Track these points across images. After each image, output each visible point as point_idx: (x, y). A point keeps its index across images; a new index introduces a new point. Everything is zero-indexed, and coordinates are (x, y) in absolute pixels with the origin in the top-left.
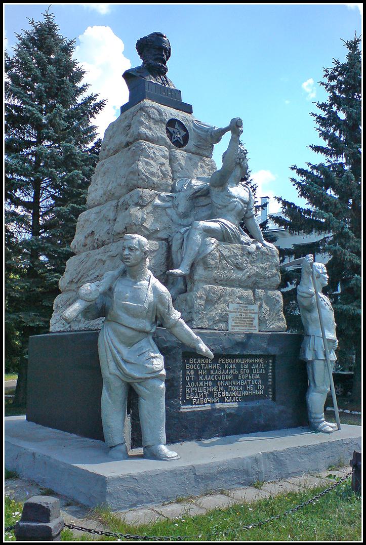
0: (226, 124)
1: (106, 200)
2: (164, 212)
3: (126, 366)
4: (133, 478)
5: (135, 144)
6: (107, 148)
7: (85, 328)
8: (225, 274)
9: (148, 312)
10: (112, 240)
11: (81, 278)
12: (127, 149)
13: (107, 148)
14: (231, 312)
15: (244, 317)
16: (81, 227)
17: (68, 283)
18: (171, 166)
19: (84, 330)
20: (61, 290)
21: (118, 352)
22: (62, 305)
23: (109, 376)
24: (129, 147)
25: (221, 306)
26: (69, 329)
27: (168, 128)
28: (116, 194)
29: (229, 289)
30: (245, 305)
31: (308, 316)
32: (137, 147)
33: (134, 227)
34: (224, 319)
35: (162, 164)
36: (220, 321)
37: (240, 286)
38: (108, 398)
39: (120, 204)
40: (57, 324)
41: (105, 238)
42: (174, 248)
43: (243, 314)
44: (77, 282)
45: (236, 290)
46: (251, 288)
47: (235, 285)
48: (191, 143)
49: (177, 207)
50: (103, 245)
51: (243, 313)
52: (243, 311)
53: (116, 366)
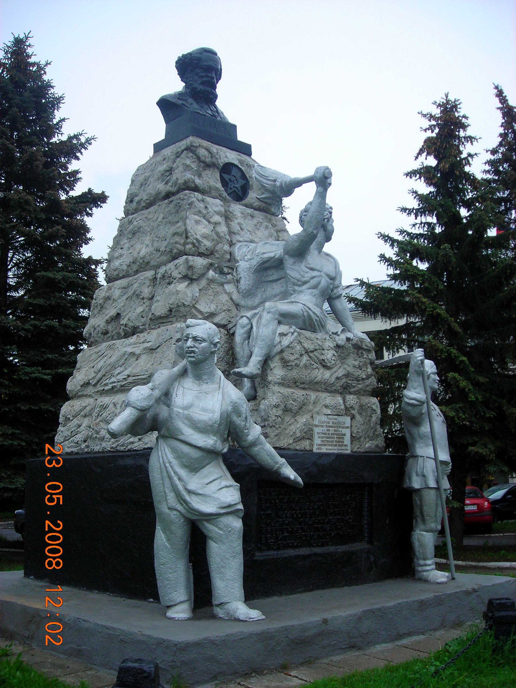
0: (310, 172)
1: (137, 270)
2: (221, 287)
3: (190, 498)
4: (212, 642)
5: (181, 195)
6: (137, 199)
7: (112, 448)
8: (305, 375)
9: (220, 425)
10: (147, 326)
11: (101, 379)
12: (166, 201)
13: (137, 199)
14: (317, 426)
15: (333, 432)
16: (99, 307)
17: (81, 386)
18: (228, 226)
19: (110, 451)
20: (71, 396)
21: (180, 479)
22: (73, 416)
23: (167, 511)
24: (170, 199)
25: (303, 419)
26: (86, 450)
27: (223, 175)
28: (153, 263)
29: (313, 396)
30: (333, 417)
31: (414, 431)
32: (183, 200)
33: (182, 309)
34: (308, 435)
35: (216, 224)
36: (303, 438)
37: (326, 390)
38: (165, 541)
39: (159, 276)
40: (66, 442)
41: (138, 324)
42: (238, 339)
43: (331, 429)
44: (95, 385)
45: (323, 395)
46: (341, 393)
47: (320, 389)
48: (253, 196)
49: (238, 281)
50: (134, 334)
51: (331, 427)
52: (331, 424)
53: (177, 497)
